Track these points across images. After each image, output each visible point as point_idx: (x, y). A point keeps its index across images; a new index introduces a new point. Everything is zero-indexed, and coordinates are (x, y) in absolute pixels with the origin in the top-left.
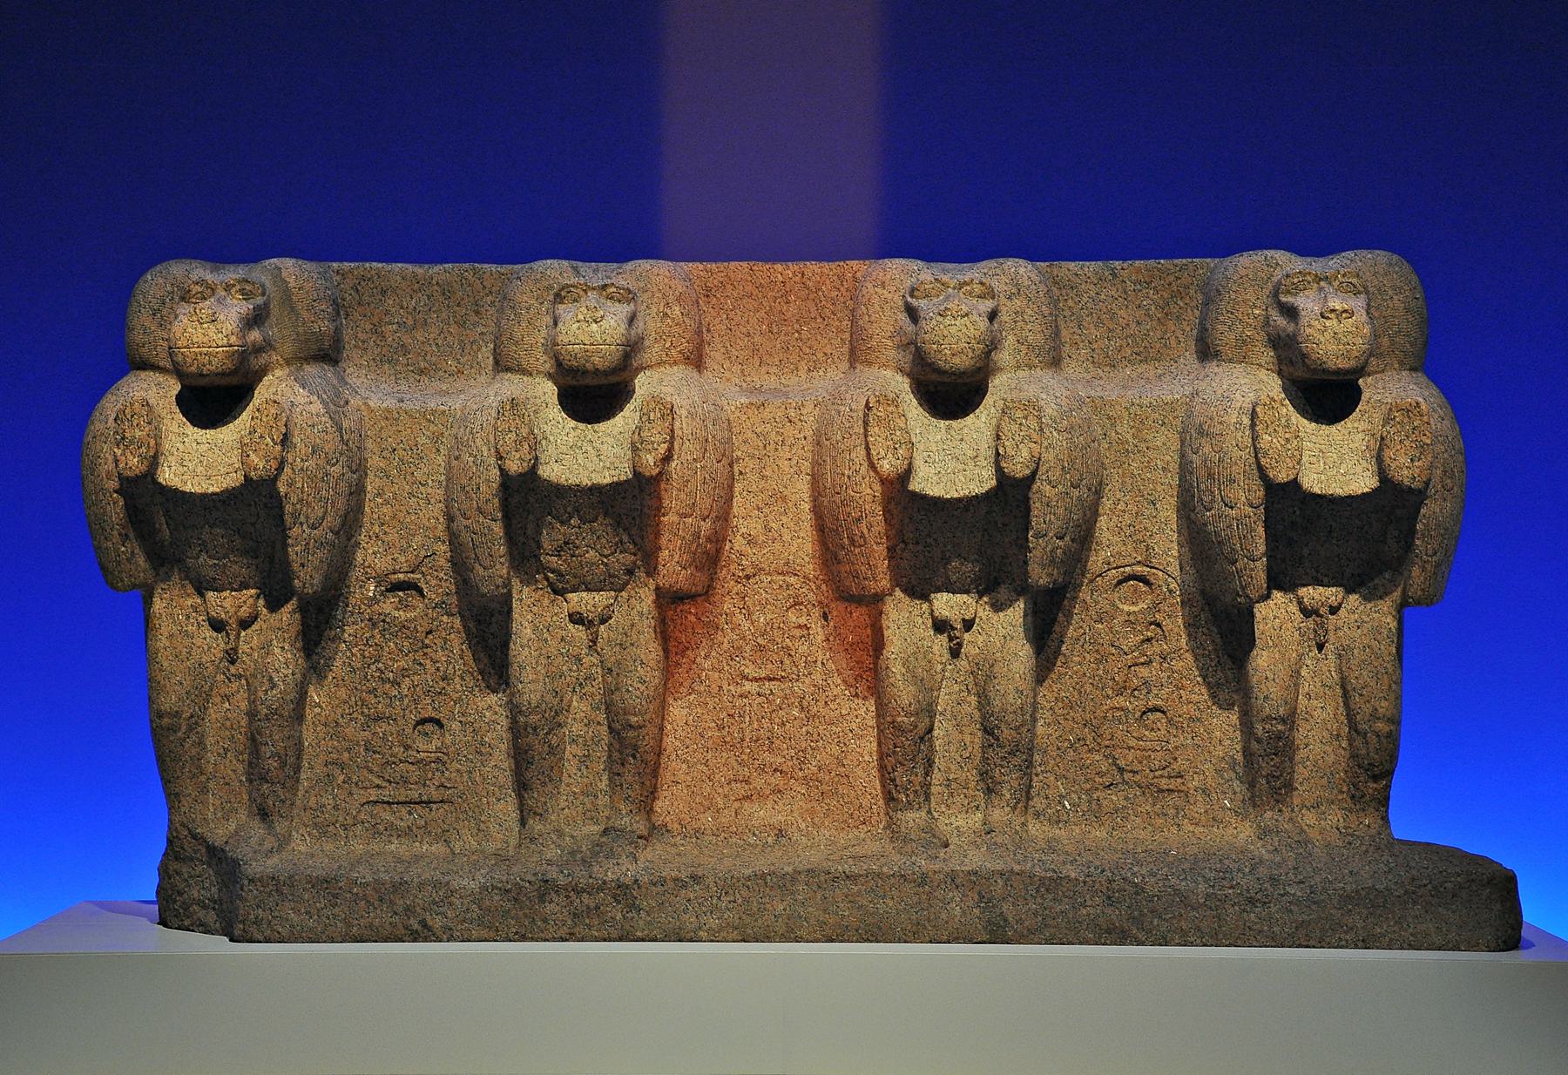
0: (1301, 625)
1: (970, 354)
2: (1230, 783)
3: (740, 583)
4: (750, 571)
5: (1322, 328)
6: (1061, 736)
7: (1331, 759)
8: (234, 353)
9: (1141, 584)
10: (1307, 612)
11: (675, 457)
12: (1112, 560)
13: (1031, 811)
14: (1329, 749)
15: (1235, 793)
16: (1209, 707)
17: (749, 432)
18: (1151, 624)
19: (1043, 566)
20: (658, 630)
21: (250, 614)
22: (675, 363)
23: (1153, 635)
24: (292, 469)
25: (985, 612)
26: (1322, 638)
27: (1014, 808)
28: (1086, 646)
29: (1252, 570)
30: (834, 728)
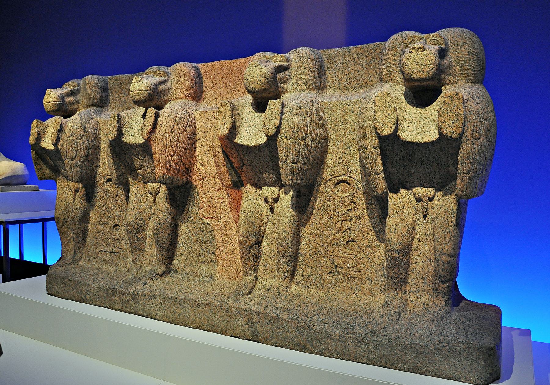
0: (416, 206)
1: (259, 83)
2: (381, 277)
3: (201, 181)
4: (203, 176)
5: (409, 57)
6: (311, 250)
7: (426, 270)
8: (55, 104)
9: (347, 184)
10: (419, 200)
11: (157, 132)
12: (333, 173)
13: (294, 281)
14: (425, 265)
15: (382, 282)
16: (375, 241)
17: (202, 122)
18: (351, 202)
19: (287, 176)
20: (168, 198)
21: (77, 188)
22: (183, 98)
23: (352, 208)
24: (63, 141)
25: (282, 195)
26: (424, 212)
27: (284, 280)
28: (324, 211)
29: (377, 179)
30: (231, 239)
